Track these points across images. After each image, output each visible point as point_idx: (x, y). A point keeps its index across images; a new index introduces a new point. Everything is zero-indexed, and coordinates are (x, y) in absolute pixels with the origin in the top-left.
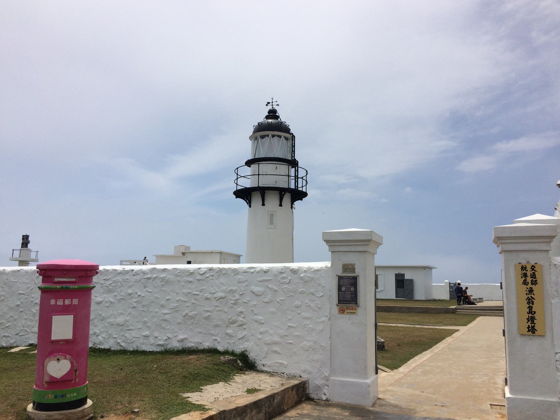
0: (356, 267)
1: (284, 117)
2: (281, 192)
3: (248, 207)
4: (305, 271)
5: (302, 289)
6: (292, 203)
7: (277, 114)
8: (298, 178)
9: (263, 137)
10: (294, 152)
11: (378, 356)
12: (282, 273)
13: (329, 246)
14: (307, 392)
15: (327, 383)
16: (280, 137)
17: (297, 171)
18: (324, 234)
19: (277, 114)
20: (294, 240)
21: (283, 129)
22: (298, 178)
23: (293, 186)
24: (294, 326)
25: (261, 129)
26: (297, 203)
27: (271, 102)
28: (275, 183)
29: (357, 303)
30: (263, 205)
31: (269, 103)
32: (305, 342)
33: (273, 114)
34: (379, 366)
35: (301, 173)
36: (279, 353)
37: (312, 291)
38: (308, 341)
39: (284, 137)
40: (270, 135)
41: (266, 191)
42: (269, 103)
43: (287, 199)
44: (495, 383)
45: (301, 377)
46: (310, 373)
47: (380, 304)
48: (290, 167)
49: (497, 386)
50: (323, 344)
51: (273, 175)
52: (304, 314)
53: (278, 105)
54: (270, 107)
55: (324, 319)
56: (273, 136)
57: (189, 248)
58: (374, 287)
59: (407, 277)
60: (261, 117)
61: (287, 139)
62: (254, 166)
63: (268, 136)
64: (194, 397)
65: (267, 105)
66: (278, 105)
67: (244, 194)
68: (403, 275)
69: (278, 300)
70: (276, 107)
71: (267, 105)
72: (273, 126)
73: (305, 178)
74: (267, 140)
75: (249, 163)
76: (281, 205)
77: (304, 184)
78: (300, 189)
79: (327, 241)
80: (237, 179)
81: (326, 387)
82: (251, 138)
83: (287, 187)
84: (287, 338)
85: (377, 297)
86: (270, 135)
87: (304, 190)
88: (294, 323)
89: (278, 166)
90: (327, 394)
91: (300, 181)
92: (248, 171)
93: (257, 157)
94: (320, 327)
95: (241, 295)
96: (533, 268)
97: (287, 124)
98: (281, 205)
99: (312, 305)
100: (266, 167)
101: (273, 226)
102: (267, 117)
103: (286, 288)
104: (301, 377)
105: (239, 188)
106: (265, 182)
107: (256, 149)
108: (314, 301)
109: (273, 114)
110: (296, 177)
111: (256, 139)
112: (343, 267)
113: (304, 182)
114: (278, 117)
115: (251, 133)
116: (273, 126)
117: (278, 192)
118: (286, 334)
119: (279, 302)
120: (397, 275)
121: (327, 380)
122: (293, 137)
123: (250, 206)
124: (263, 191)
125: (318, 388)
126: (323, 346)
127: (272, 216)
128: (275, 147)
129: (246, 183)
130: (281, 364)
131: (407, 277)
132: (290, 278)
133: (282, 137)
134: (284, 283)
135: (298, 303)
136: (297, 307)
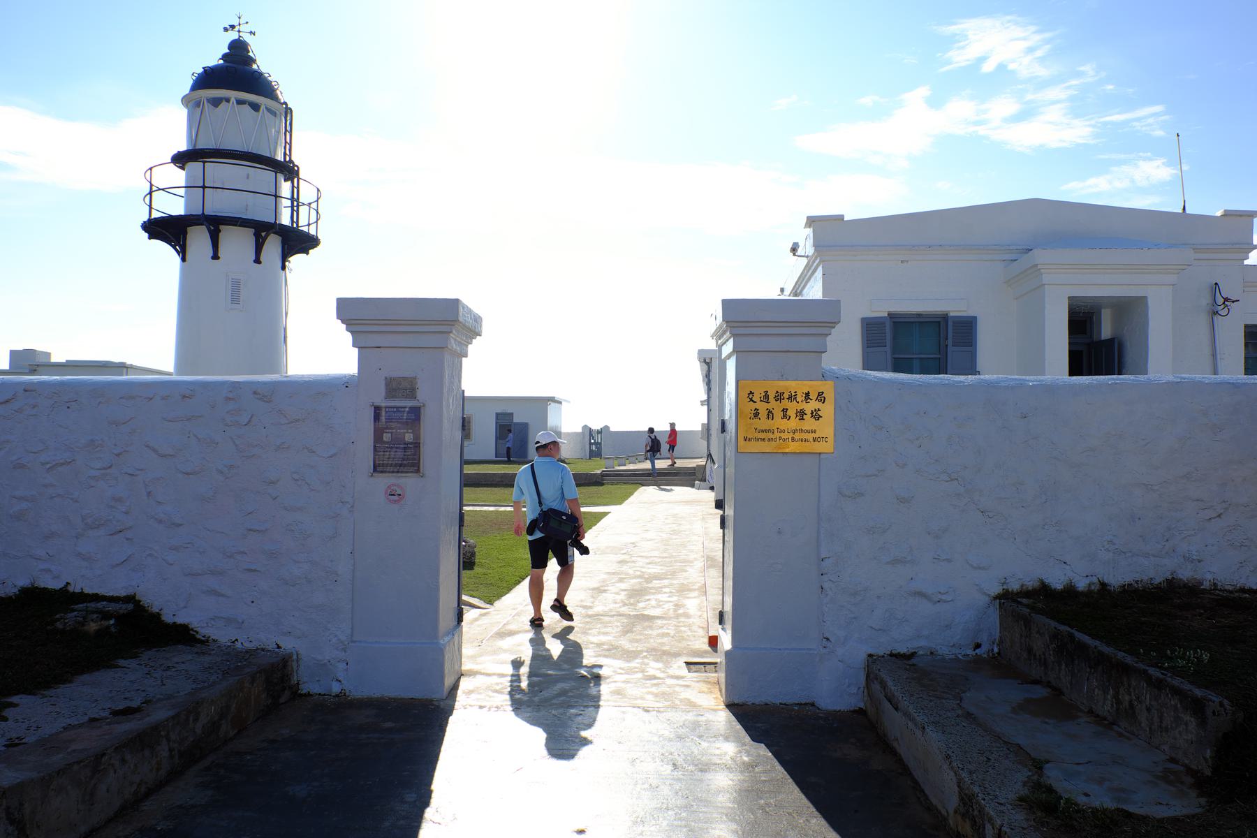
0: (419, 385)
1: (265, 61)
3: (177, 259)
6: (284, 258)
7: (255, 66)
9: (216, 102)
10: (290, 144)
11: (464, 581)
13: (352, 332)
14: (294, 680)
16: (255, 107)
17: (295, 189)
19: (255, 66)
23: (285, 220)
25: (208, 79)
26: (296, 260)
27: (236, 23)
29: (418, 471)
30: (215, 257)
33: (238, 53)
34: (464, 598)
35: (306, 194)
39: (268, 109)
40: (233, 100)
41: (221, 227)
42: (233, 27)
43: (273, 246)
44: (687, 615)
47: (469, 469)
48: (281, 177)
49: (691, 621)
51: (234, 189)
53: (252, 33)
54: (233, 35)
56: (240, 102)
57: (48, 355)
58: (458, 434)
60: (213, 55)
62: (196, 166)
63: (228, 100)
66: (252, 33)
67: (163, 229)
70: (246, 38)
71: (226, 30)
75: (180, 159)
76: (257, 261)
77: (313, 219)
78: (305, 229)
80: (150, 193)
83: (200, 213)
85: (466, 457)
86: (233, 100)
87: (313, 232)
91: (303, 211)
92: (178, 176)
93: (200, 146)
95: (118, 455)
100: (218, 171)
102: (225, 57)
105: (155, 215)
106: (218, 204)
107: (195, 125)
109: (238, 53)
110: (295, 202)
111: (198, 104)
112: (387, 385)
113: (313, 213)
115: (186, 89)
116: (234, 76)
122: (288, 111)
123: (183, 259)
124: (215, 224)
128: (235, 123)
129: (175, 207)
133: (263, 107)
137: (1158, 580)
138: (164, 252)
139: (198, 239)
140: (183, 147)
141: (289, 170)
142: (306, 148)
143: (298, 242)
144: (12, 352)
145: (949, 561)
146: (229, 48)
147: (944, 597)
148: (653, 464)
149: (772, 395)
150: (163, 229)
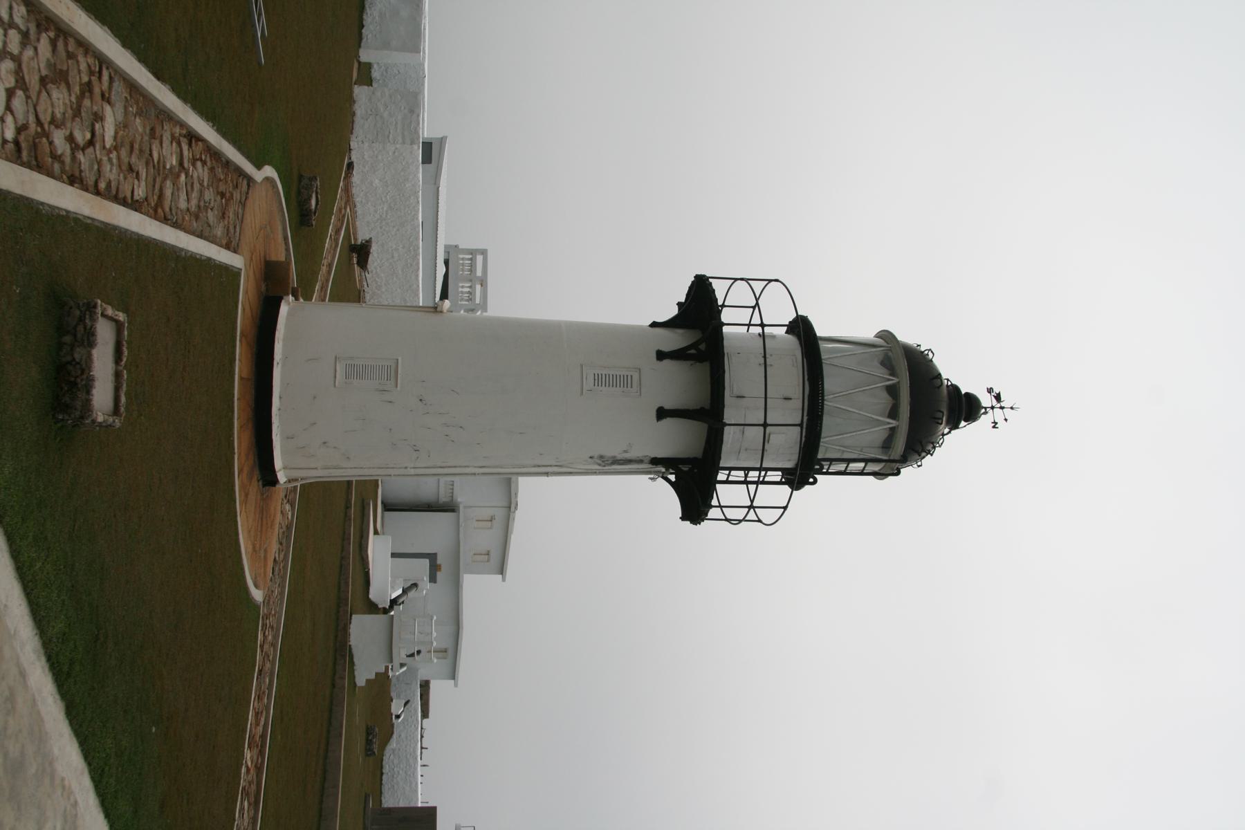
1: (958, 444)
2: (709, 415)
7: (963, 423)
16: (893, 413)
19: (963, 423)
20: (544, 478)
21: (918, 444)
25: (918, 366)
26: (662, 496)
28: (736, 392)
30: (661, 355)
33: (965, 408)
39: (893, 431)
42: (998, 398)
43: (677, 439)
51: (761, 401)
54: (986, 400)
56: (892, 391)
60: (956, 369)
61: (887, 444)
64: (363, 675)
65: (990, 390)
67: (701, 304)
70: (984, 421)
71: (990, 390)
72: (921, 406)
73: (752, 516)
74: (882, 372)
75: (801, 327)
76: (662, 414)
77: (730, 513)
78: (715, 502)
82: (886, 336)
83: (726, 420)
86: (895, 380)
92: (778, 313)
93: (823, 346)
98: (662, 414)
100: (788, 377)
102: (955, 389)
106: (741, 378)
109: (965, 408)
113: (740, 514)
114: (955, 426)
116: (921, 406)
117: (707, 406)
127: (622, 382)
128: (856, 412)
129: (734, 320)
133: (893, 423)
140: (821, 329)
141: (798, 477)
143: (695, 505)
146: (967, 394)
150: (701, 304)
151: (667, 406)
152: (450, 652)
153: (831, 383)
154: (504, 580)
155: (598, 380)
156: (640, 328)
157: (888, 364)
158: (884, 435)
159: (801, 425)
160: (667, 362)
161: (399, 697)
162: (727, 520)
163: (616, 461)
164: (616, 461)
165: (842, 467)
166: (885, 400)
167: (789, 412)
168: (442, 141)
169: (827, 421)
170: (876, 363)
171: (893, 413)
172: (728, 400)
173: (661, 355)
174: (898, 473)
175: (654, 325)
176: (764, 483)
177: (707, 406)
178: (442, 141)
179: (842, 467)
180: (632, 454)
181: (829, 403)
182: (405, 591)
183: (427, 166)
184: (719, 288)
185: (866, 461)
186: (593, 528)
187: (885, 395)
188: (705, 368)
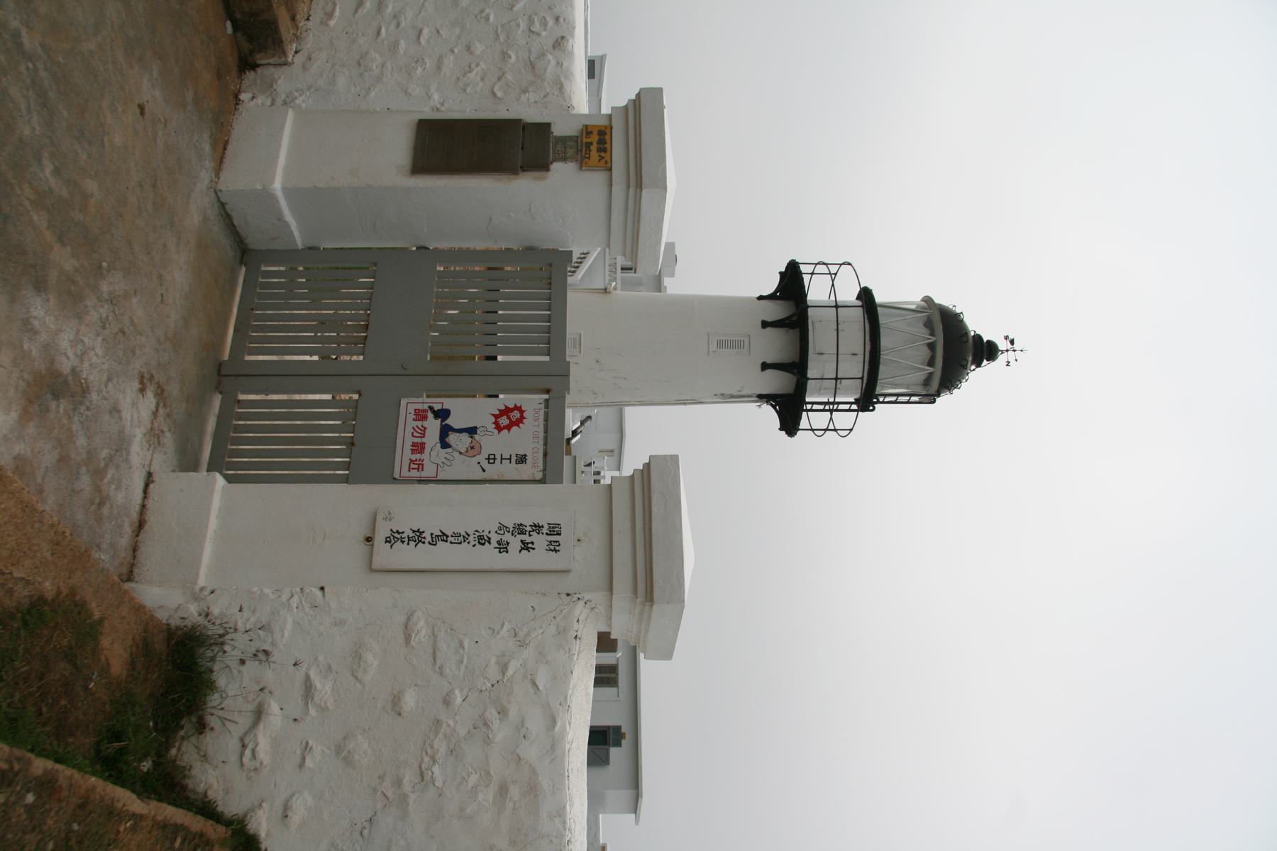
1: (979, 378)
2: (797, 367)
4: (559, 64)
5: (514, 57)
6: (763, 398)
7: (985, 362)
8: (831, 411)
12: (557, 19)
15: (279, 102)
16: (931, 363)
18: (657, 93)
19: (985, 362)
22: (831, 411)
24: (422, 40)
26: (769, 415)
28: (818, 350)
30: (765, 324)
31: (1012, 342)
32: (379, 60)
33: (986, 351)
35: (843, 419)
36: (356, 11)
37: (509, 77)
38: (383, 65)
39: (931, 374)
42: (1012, 342)
43: (777, 382)
45: (296, 52)
46: (304, 68)
50: (372, 94)
51: (835, 352)
52: (449, 61)
54: (1002, 345)
55: (436, 97)
56: (931, 346)
57: (667, 654)
59: (614, 751)
60: (978, 324)
61: (927, 382)
65: (1006, 338)
67: (792, 281)
68: (618, 744)
69: (487, 11)
70: (1002, 358)
71: (1006, 338)
72: (954, 350)
74: (923, 332)
75: (866, 295)
76: (765, 366)
79: (636, 103)
81: (268, 102)
82: (928, 300)
83: (809, 375)
84: (393, 26)
86: (933, 339)
88: (428, 42)
89: (860, 358)
90: (252, 104)
92: (848, 294)
94: (416, 91)
96: (556, 551)
97: (964, 385)
98: (765, 366)
99: (472, 75)
100: (855, 337)
101: (713, 347)
102: (978, 338)
103: (518, 25)
104: (296, 52)
108: (482, 79)
109: (986, 351)
114: (979, 365)
116: (954, 350)
117: (797, 360)
118: (403, 25)
119: (482, 11)
120: (617, 729)
121: (285, 103)
122: (930, 398)
125: (269, 87)
126: (368, 94)
127: (737, 345)
128: (905, 352)
129: (817, 291)
130: (330, 15)
131: (614, 751)
132: (544, 34)
133: (931, 369)
134: (531, 21)
135: (479, 48)
136: (468, 48)
137: (220, 809)
138: (770, 284)
139: (776, 311)
140: (879, 298)
141: (866, 402)
142: (893, 419)
143: (790, 425)
144: (660, 91)
145: (302, 765)
146: (988, 342)
147: (248, 752)
148: (509, 418)
149: (593, 468)
150: (792, 281)
151: (769, 361)
152: (616, 452)
153: (885, 342)
154: (637, 821)
155: (720, 344)
156: (750, 298)
157: (929, 324)
158: (924, 378)
159: (862, 378)
160: (769, 329)
161: (575, 406)
162: (812, 430)
163: (732, 396)
164: (732, 396)
165: (893, 399)
166: (926, 353)
167: (854, 367)
168: (603, 58)
169: (882, 368)
170: (921, 325)
171: (931, 363)
172: (811, 356)
173: (765, 324)
174: (934, 402)
175: (761, 298)
176: (837, 410)
177: (797, 360)
178: (603, 58)
179: (893, 399)
180: (745, 392)
181: (884, 356)
182: (582, 423)
183: (608, 691)
184: (803, 268)
185: (911, 395)
186: (714, 446)
187: (926, 348)
188: (793, 334)
